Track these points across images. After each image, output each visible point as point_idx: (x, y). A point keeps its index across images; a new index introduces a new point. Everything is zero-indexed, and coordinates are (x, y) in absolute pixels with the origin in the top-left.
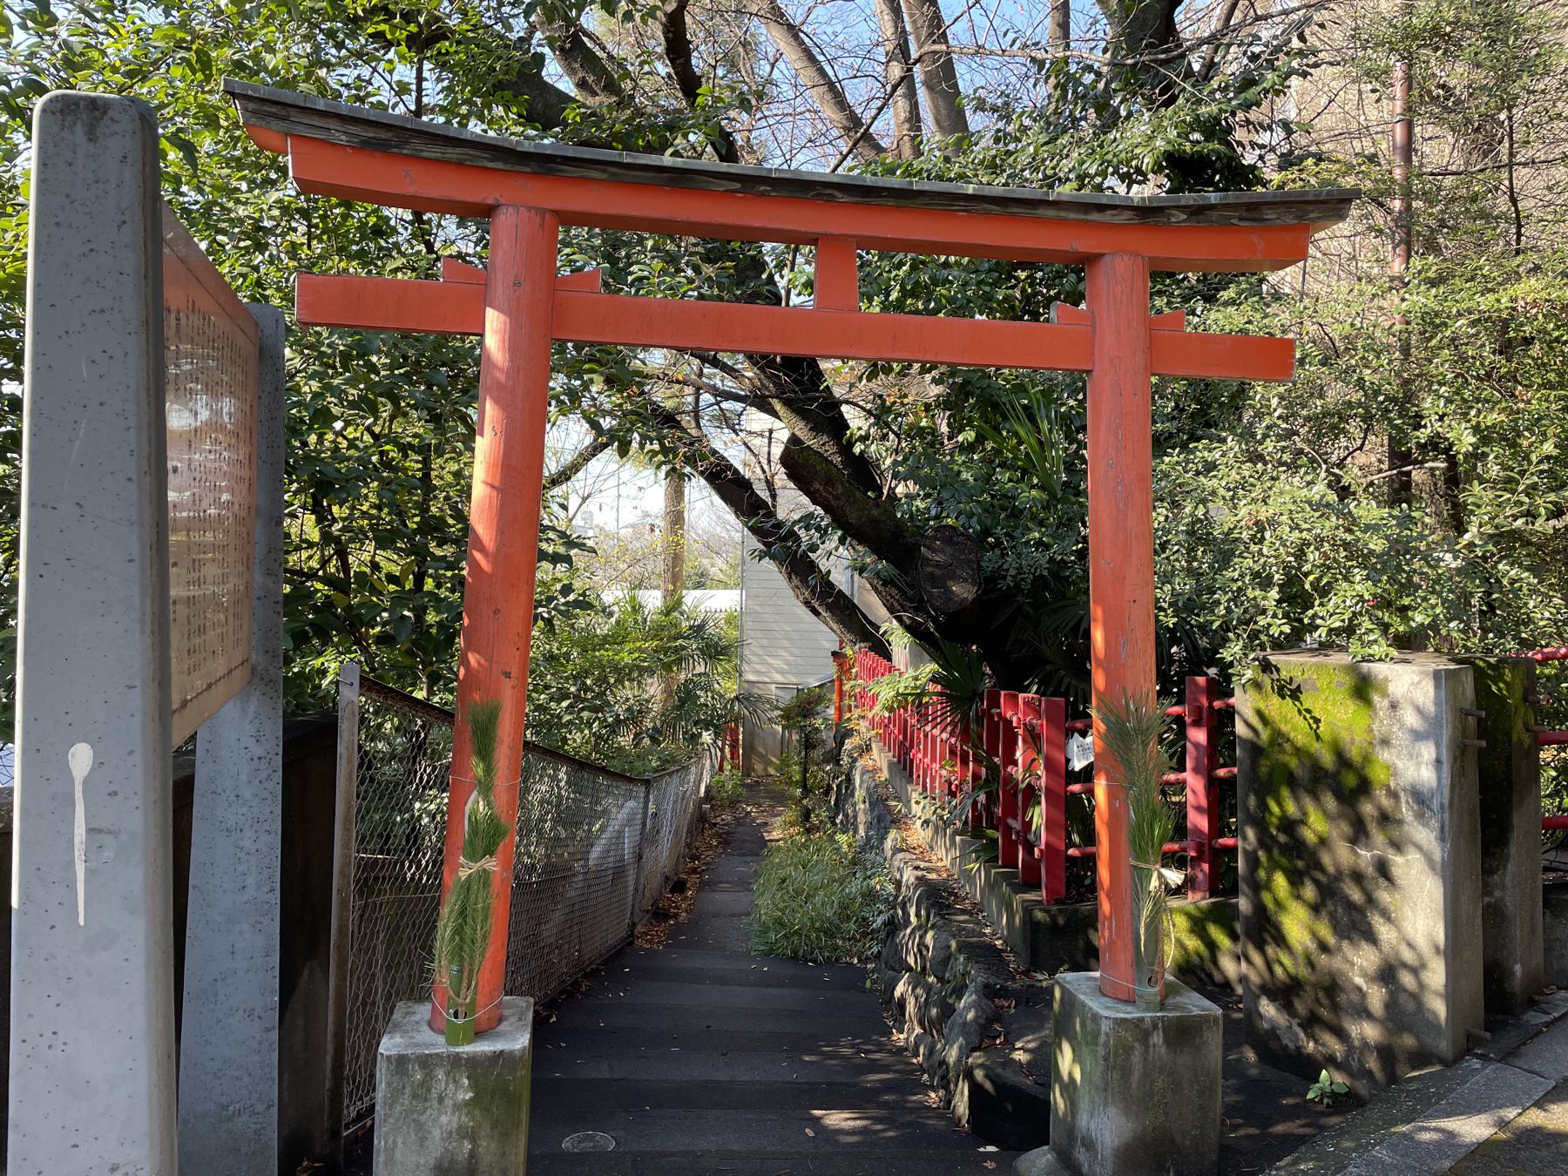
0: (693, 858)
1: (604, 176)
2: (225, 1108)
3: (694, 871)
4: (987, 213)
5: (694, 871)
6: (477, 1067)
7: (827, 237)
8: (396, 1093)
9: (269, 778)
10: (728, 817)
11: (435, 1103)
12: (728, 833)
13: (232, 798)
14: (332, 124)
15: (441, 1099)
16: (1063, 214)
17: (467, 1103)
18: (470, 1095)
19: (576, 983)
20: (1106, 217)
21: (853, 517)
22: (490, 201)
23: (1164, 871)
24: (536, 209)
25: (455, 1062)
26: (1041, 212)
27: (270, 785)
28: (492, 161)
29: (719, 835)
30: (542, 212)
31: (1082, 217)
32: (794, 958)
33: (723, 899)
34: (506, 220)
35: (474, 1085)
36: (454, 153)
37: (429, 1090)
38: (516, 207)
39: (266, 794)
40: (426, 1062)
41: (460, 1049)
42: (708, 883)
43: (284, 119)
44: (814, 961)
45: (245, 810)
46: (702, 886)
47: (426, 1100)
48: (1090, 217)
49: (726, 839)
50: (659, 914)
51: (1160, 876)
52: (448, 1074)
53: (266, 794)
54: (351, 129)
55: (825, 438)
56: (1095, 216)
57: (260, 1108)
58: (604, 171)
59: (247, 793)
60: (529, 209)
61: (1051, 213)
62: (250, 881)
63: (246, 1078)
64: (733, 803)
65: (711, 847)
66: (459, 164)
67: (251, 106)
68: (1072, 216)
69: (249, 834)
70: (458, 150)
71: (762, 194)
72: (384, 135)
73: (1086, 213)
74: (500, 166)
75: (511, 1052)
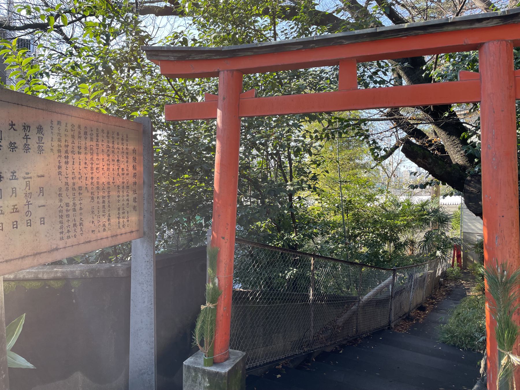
0: (433, 298)
1: (252, 54)
2: (141, 370)
3: (432, 303)
4: (417, 35)
5: (432, 303)
6: (212, 376)
7: (342, 60)
8: (188, 378)
9: (150, 268)
10: (452, 284)
11: (198, 384)
12: (451, 291)
13: (141, 274)
14: (170, 54)
15: (200, 384)
16: (458, 27)
17: (208, 387)
18: (208, 385)
19: (356, 340)
20: (484, 24)
21: (438, 172)
22: (216, 70)
23: (511, 356)
24: (230, 70)
25: (204, 371)
26: (445, 29)
27: (150, 270)
28: (215, 56)
29: (447, 291)
30: (232, 71)
31: (469, 27)
32: (454, 346)
33: (441, 317)
34: (222, 74)
35: (210, 382)
36: (204, 56)
37: (196, 380)
38: (224, 71)
39: (149, 273)
40: (196, 370)
41: (205, 368)
42: (436, 309)
43: (157, 55)
44: (463, 349)
45: (144, 277)
46: (434, 310)
47: (196, 383)
48: (473, 26)
49: (449, 293)
50: (408, 318)
51: (509, 358)
52: (202, 375)
53: (149, 273)
54: (175, 54)
55: (454, 137)
56: (477, 25)
57: (150, 373)
58: (252, 52)
59: (144, 272)
60: (227, 71)
61: (451, 28)
62: (146, 300)
63: (146, 363)
64: (456, 279)
65: (442, 295)
66: (206, 59)
67: (149, 53)
68: (463, 27)
69: (145, 285)
70: (205, 55)
71: (312, 48)
72: (184, 54)
73: (471, 24)
74: (218, 57)
75: (221, 373)
